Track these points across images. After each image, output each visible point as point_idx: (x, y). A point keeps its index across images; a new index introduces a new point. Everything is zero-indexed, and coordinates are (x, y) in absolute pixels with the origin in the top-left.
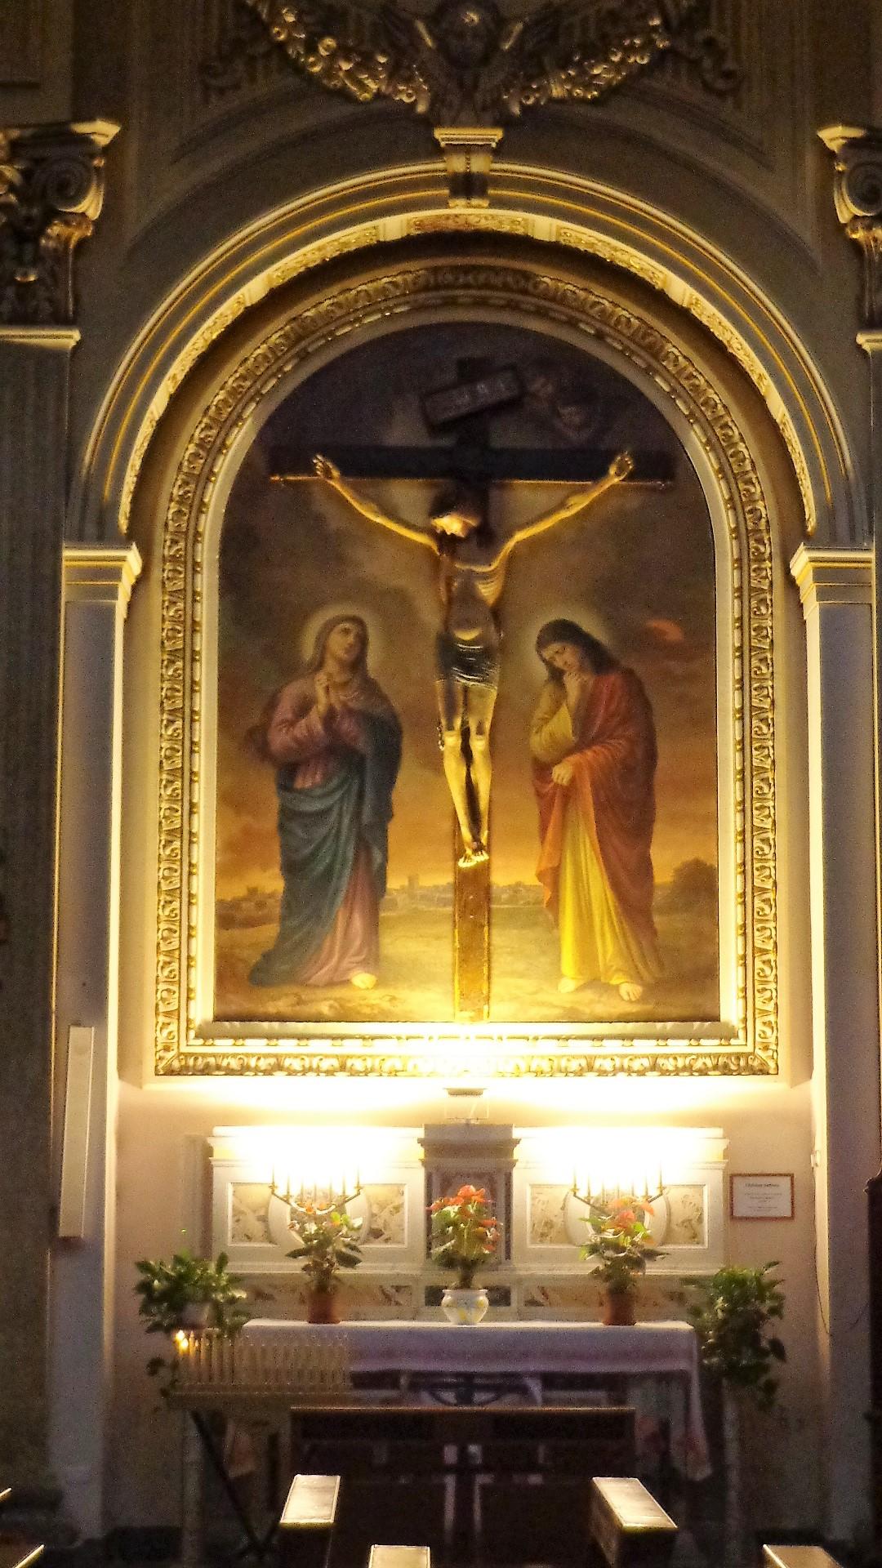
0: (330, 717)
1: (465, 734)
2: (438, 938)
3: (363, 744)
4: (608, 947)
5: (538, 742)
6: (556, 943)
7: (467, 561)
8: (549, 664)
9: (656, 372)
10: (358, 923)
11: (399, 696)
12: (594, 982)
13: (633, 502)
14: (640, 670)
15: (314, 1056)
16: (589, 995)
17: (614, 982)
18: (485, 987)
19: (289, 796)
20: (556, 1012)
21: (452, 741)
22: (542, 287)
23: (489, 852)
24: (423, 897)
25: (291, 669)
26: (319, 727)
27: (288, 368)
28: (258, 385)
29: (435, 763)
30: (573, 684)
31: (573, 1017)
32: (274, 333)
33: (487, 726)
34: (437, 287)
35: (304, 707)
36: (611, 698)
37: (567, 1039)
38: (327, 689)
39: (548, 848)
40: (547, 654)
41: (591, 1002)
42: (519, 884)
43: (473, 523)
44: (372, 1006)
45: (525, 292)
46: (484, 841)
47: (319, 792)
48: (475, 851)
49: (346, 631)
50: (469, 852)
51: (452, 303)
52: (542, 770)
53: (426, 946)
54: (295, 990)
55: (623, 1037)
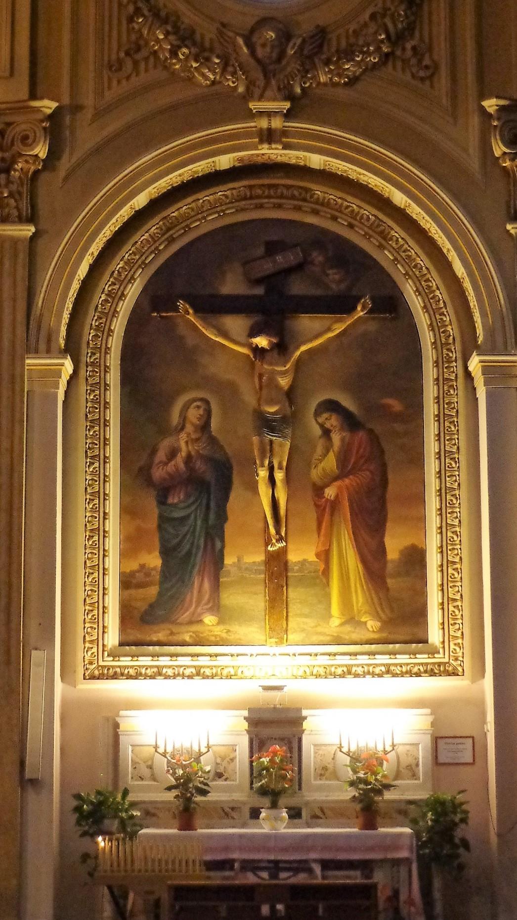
0: (189, 459)
1: (271, 469)
2: (256, 594)
3: (210, 476)
4: (359, 598)
5: (316, 474)
6: (328, 597)
7: (271, 364)
8: (322, 426)
9: (385, 248)
10: (207, 585)
11: (231, 446)
12: (351, 620)
13: (372, 327)
14: (378, 429)
15: (181, 666)
16: (348, 628)
17: (363, 619)
18: (285, 622)
19: (164, 507)
20: (328, 638)
21: (263, 473)
22: (316, 196)
23: (286, 542)
24: (246, 569)
25: (164, 430)
26: (182, 466)
27: (161, 247)
28: (143, 258)
29: (253, 487)
30: (336, 438)
31: (338, 641)
32: (153, 226)
33: (285, 464)
34: (251, 198)
35: (173, 453)
36: (359, 447)
37: (335, 655)
38: (187, 442)
39: (322, 538)
40: (320, 420)
41: (349, 632)
42: (305, 560)
43: (274, 340)
44: (216, 636)
45: (305, 200)
46: (283, 534)
47: (182, 505)
48: (277, 541)
49: (198, 407)
50: (274, 541)
51: (261, 207)
52: (318, 490)
53: (246, 598)
54: (170, 626)
55: (350, 654)
